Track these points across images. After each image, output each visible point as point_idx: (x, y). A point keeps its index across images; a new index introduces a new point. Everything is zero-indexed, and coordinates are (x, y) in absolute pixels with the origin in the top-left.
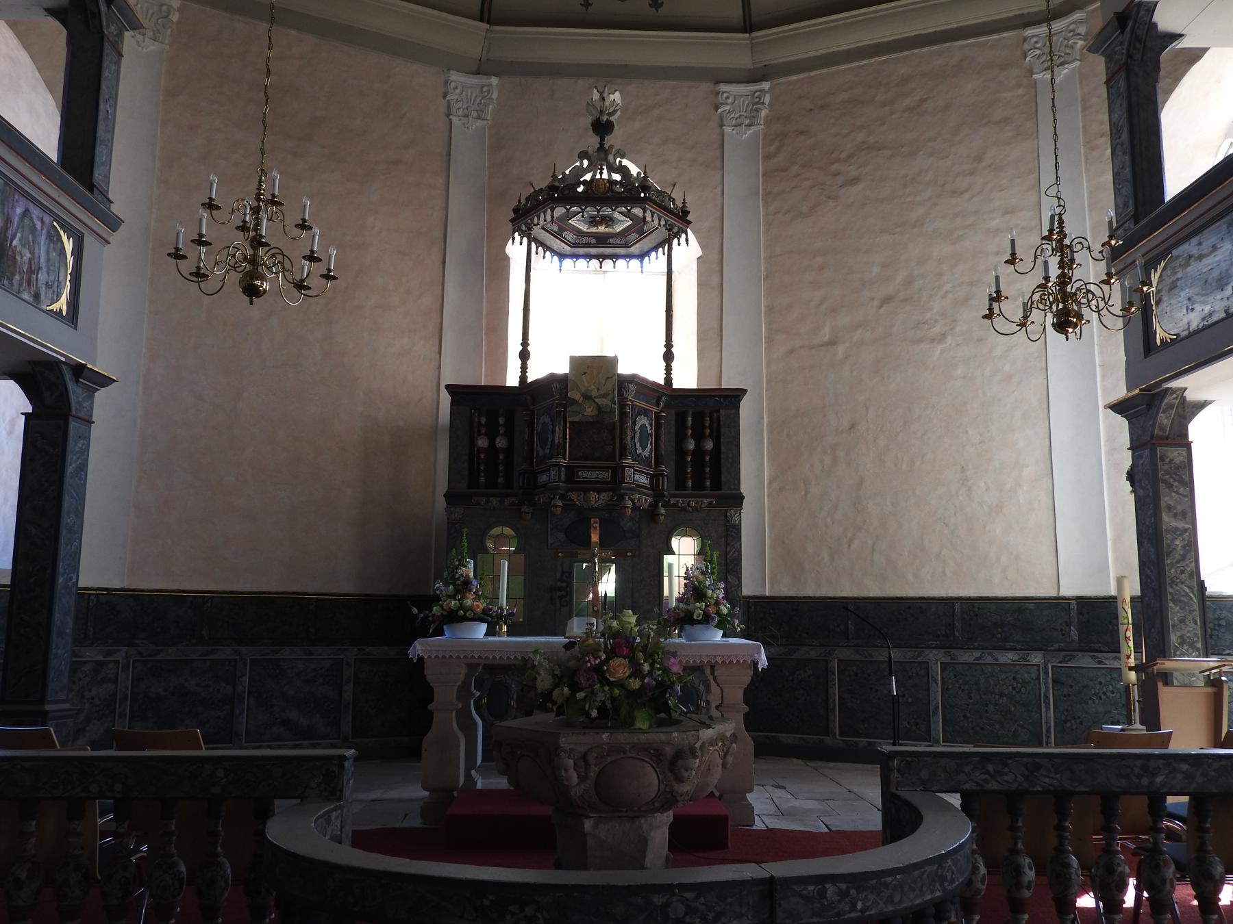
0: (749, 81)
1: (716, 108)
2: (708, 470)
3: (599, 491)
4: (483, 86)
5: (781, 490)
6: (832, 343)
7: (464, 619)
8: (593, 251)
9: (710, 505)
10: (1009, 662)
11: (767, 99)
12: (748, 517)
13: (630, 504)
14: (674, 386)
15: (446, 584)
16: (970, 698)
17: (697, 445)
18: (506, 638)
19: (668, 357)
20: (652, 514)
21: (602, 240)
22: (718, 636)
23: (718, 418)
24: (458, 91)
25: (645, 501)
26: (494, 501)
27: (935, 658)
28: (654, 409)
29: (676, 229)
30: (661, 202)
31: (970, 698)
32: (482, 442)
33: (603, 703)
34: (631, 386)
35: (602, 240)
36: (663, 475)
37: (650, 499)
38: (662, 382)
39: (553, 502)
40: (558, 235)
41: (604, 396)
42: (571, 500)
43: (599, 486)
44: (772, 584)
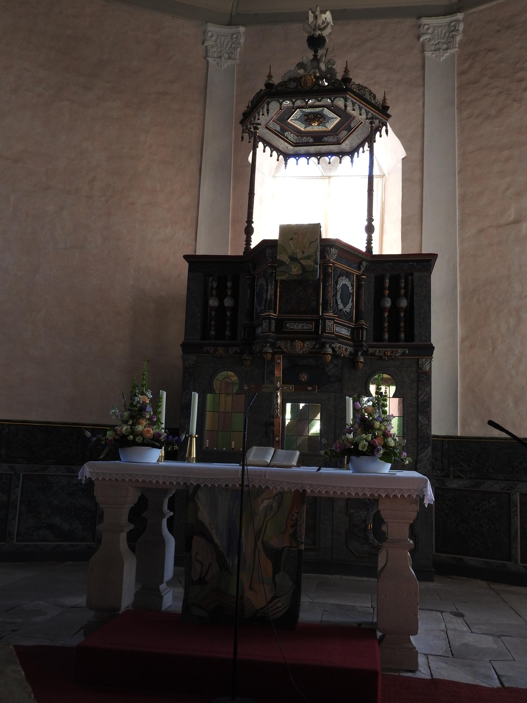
0: (445, 14)
1: (419, 37)
2: (402, 324)
3: (303, 340)
4: (233, 34)
5: (472, 347)
6: (517, 221)
7: (134, 444)
8: (312, 149)
9: (404, 354)
11: (461, 27)
12: (439, 366)
13: (330, 351)
14: (373, 254)
17: (394, 303)
18: (194, 465)
19: (370, 229)
20: (352, 361)
21: (318, 139)
22: (386, 468)
23: (412, 279)
24: (214, 38)
25: (346, 350)
26: (220, 350)
28: (356, 272)
29: (377, 122)
30: (363, 97)
32: (213, 302)
34: (333, 250)
35: (318, 139)
36: (362, 329)
37: (350, 349)
38: (364, 250)
39: (265, 349)
40: (280, 135)
41: (308, 258)
42: (280, 348)
43: (303, 336)
44: (463, 426)
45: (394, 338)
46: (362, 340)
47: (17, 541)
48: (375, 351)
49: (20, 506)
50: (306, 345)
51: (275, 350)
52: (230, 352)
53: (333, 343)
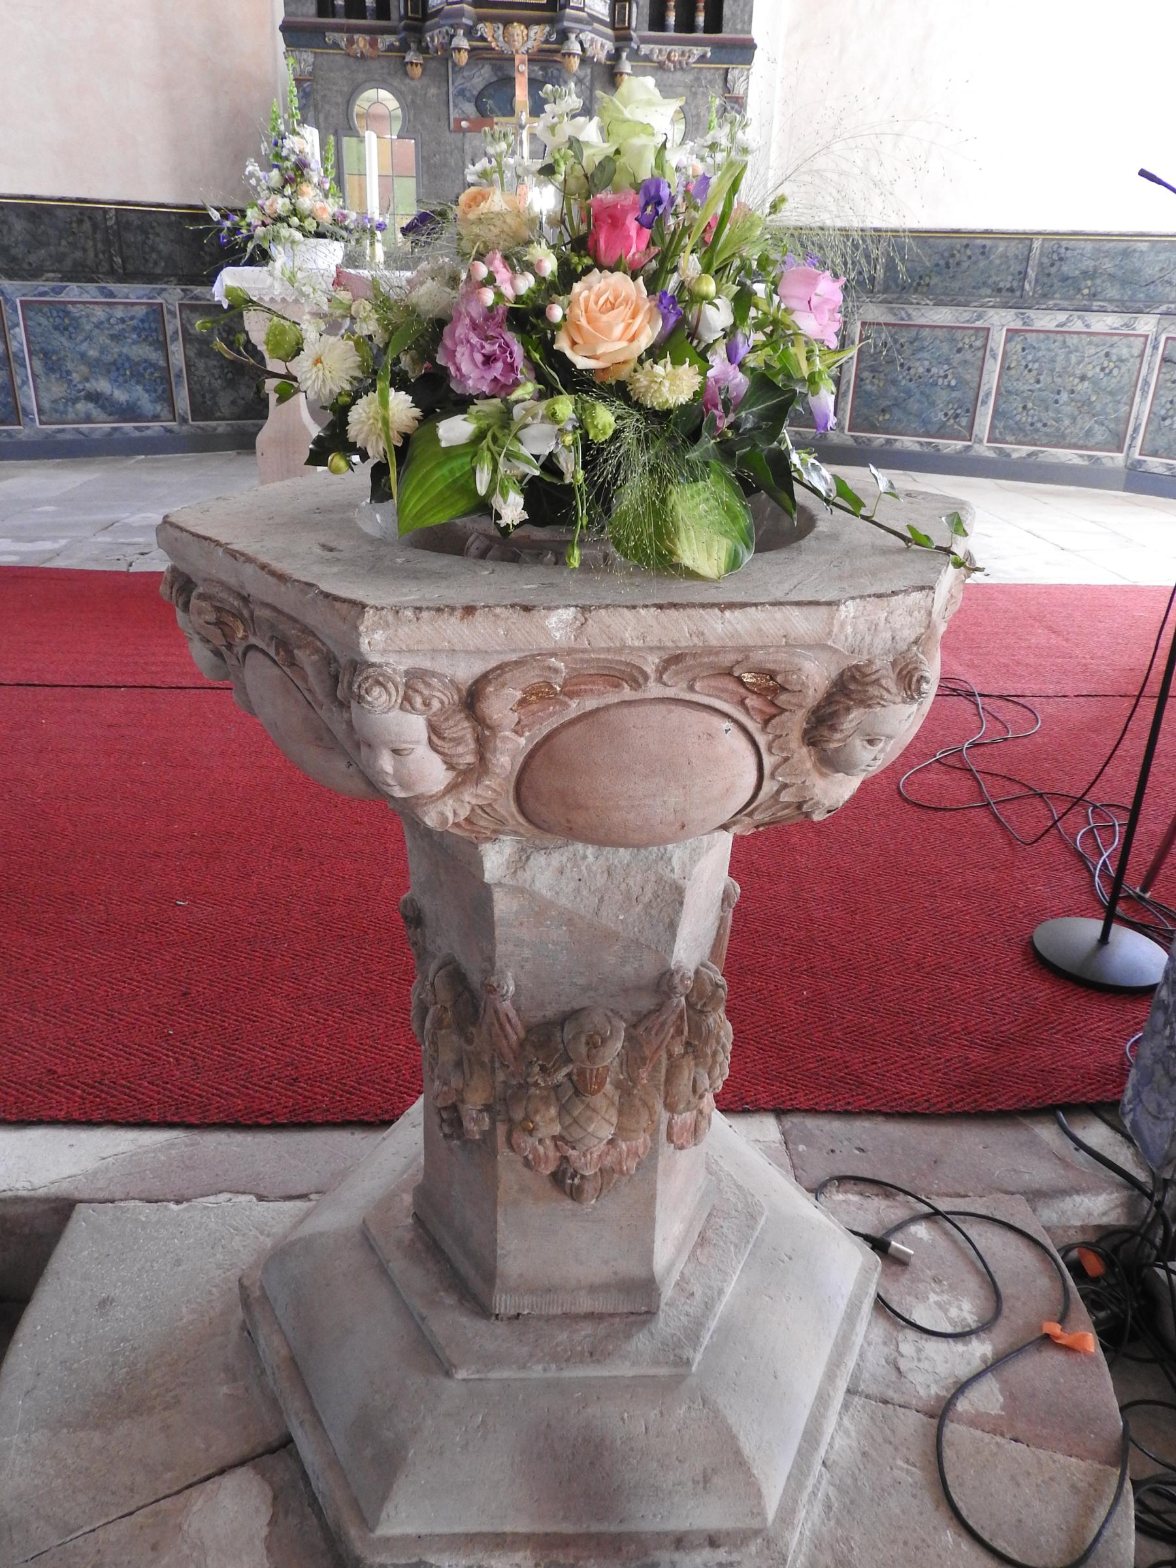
3: (528, 23)
9: (702, 59)
10: (1106, 330)
13: (576, 48)
15: (267, 167)
16: (1038, 382)
26: (361, 41)
27: (1000, 320)
31: (1038, 382)
33: (550, 465)
39: (455, 42)
45: (686, 24)
46: (629, 28)
47: (41, 423)
48: (652, 50)
49: (30, 360)
50: (532, 34)
51: (475, 43)
52: (380, 46)
53: (582, 31)
